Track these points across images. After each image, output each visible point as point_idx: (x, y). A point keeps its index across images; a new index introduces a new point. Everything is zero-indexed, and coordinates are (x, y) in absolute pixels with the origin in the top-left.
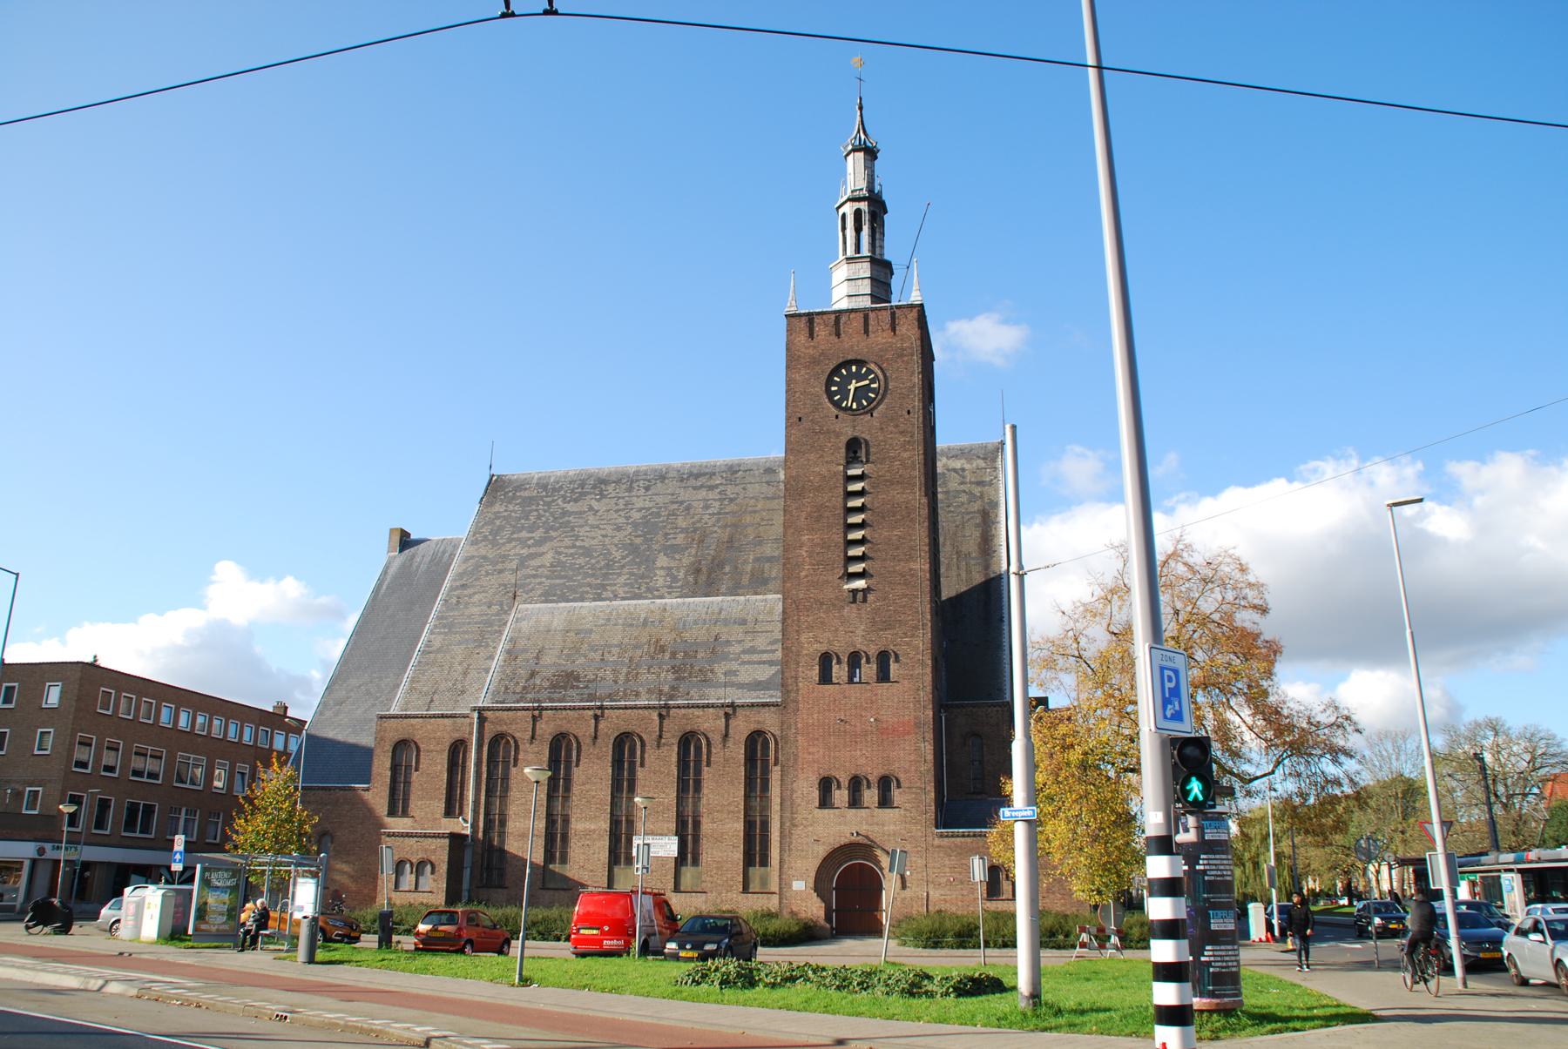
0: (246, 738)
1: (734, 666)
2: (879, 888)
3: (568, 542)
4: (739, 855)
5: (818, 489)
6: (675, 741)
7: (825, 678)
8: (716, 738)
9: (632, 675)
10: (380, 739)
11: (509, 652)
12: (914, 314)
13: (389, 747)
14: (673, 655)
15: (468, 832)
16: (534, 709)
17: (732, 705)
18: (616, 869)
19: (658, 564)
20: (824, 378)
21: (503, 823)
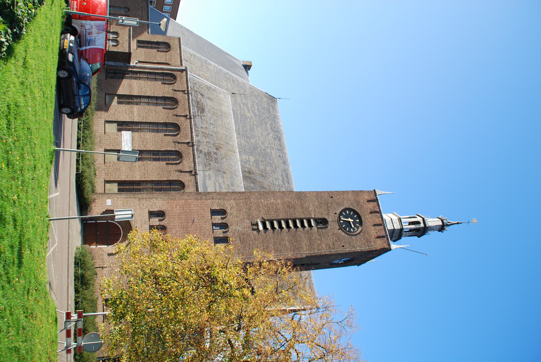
1: (213, 178)
2: (108, 244)
3: (255, 123)
4: (123, 178)
5: (302, 206)
6: (177, 149)
7: (214, 212)
8: (180, 167)
9: (205, 135)
10: (170, 38)
11: (210, 88)
12: (387, 246)
13: (166, 41)
14: (216, 153)
15: (131, 64)
16: (188, 91)
17: (196, 174)
18: (116, 125)
19: (250, 157)
20: (351, 207)
21: (135, 78)
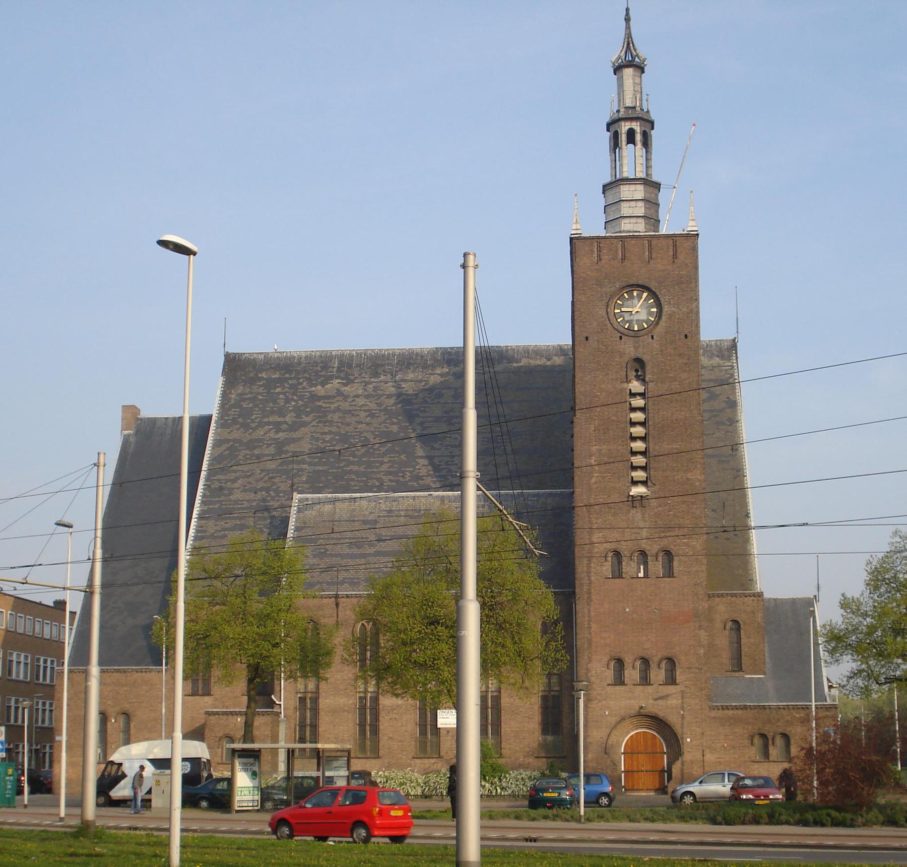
0: (37, 630)
